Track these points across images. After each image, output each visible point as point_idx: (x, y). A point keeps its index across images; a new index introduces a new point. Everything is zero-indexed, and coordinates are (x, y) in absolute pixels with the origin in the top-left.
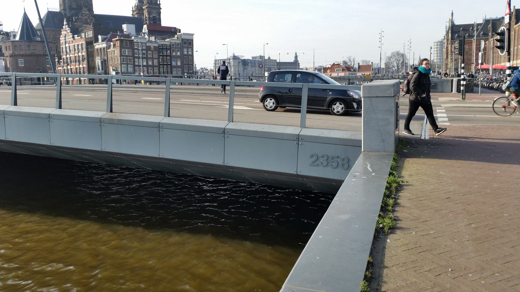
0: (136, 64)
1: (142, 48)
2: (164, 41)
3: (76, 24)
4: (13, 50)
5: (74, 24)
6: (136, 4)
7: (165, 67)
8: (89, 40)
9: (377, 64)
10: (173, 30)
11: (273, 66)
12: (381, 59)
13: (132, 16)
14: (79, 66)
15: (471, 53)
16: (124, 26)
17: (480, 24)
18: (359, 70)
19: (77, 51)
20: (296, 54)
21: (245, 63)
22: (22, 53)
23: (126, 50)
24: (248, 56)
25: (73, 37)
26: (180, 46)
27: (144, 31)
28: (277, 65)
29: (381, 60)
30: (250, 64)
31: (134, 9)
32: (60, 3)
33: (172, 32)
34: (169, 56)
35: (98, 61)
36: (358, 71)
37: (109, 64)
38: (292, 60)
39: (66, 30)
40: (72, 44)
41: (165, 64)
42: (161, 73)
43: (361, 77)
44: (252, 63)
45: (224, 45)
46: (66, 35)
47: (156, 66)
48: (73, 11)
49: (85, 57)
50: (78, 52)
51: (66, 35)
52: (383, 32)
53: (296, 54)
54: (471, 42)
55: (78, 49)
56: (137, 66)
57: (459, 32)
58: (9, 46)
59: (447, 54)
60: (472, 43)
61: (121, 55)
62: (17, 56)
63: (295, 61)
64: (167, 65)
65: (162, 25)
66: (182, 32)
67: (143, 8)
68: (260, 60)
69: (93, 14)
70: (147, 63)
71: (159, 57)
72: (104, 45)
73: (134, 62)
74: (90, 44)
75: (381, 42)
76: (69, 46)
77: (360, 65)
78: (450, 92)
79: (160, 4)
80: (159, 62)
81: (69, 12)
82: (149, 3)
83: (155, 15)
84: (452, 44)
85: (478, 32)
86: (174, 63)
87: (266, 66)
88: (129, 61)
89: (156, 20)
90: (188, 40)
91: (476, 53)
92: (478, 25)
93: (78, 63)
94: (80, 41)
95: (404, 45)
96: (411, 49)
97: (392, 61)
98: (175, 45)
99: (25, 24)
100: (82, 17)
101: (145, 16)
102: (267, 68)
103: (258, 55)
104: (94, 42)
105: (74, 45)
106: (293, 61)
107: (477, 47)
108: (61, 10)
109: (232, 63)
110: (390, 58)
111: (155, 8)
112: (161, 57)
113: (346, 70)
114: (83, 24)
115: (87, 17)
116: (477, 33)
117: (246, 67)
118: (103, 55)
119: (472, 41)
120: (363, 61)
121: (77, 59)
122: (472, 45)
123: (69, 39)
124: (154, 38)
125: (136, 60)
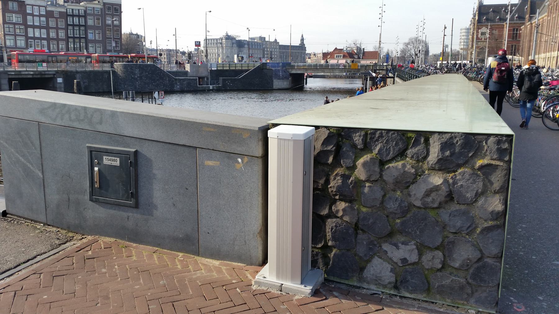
0: (29, 36)
1: (39, 13)
2: (78, 5)
7: (77, 40)
9: (391, 51)
11: (275, 49)
15: (500, 40)
17: (515, 5)
18: (363, 57)
20: (302, 36)
21: (240, 44)
23: (14, 15)
24: (244, 36)
26: (102, 12)
28: (280, 49)
30: (246, 46)
34: (83, 26)
36: (362, 59)
42: (70, 49)
43: (345, 66)
45: (140, 9)
47: (62, 40)
52: (385, 5)
53: (302, 36)
54: (503, 27)
57: (488, 13)
59: (473, 41)
60: (503, 28)
64: (80, 38)
68: (259, 41)
70: (48, 34)
75: (381, 19)
78: (250, 263)
84: (479, 29)
85: (512, 14)
86: (90, 36)
91: (508, 41)
92: (513, 5)
96: (424, 31)
97: (410, 49)
103: (258, 36)
106: (298, 45)
107: (510, 33)
110: (407, 44)
112: (70, 28)
113: (347, 57)
116: (511, 16)
117: (242, 49)
119: (504, 26)
122: (503, 31)
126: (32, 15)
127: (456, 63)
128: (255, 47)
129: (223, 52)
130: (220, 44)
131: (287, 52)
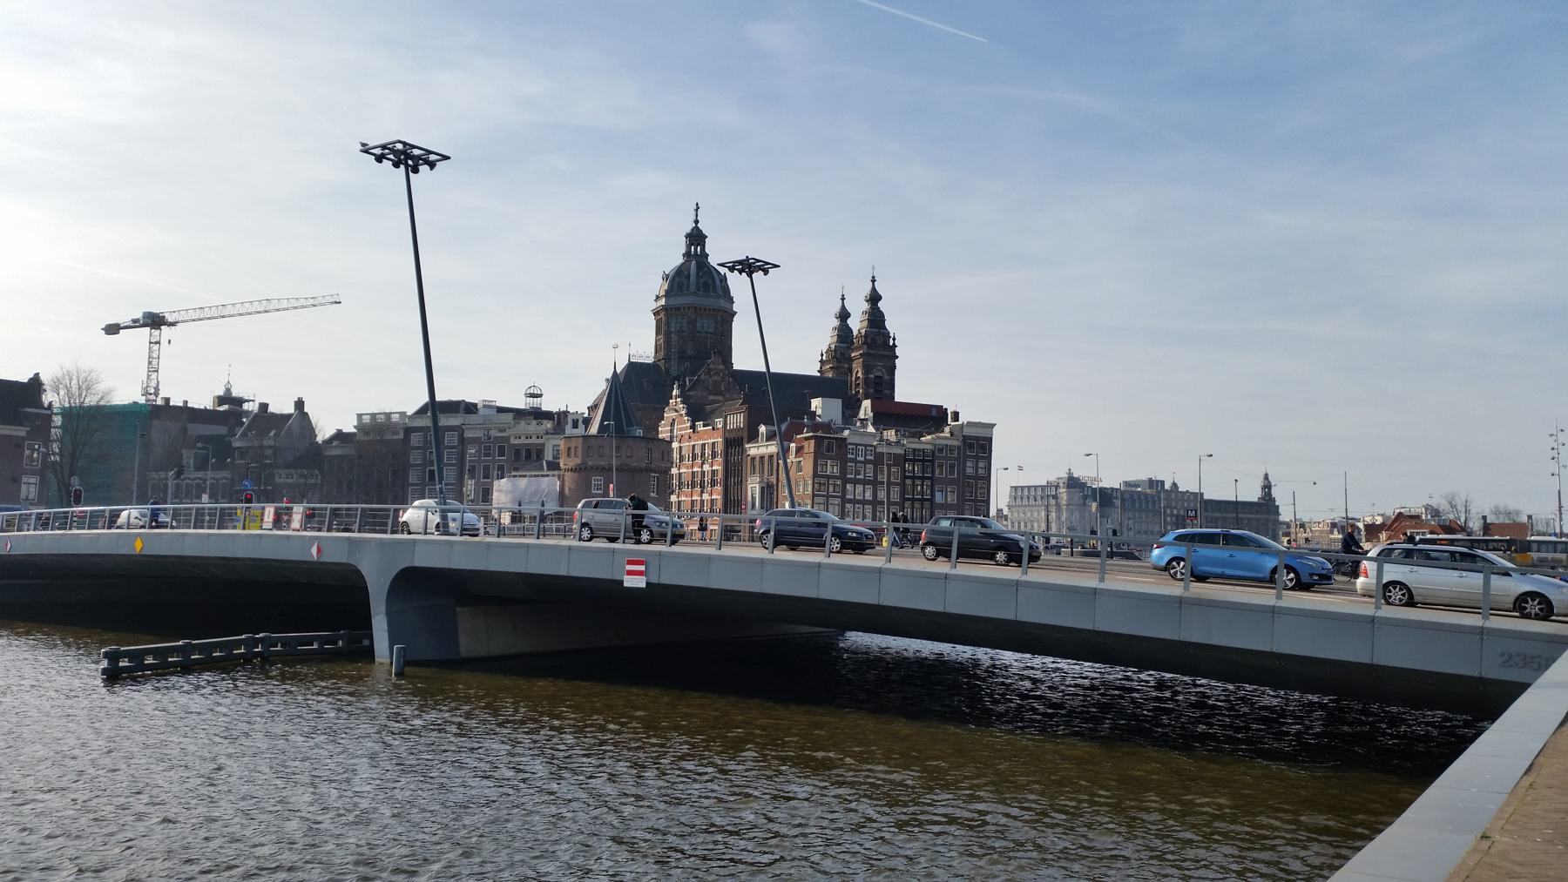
0: (847, 497)
1: (865, 458)
3: (691, 393)
4: (583, 457)
5: (688, 393)
6: (833, 346)
7: (917, 505)
8: (732, 436)
9: (1544, 521)
10: (934, 413)
12: (1560, 511)
13: (819, 374)
14: (701, 496)
16: (816, 403)
19: (699, 461)
21: (1105, 497)
22: (603, 463)
23: (829, 461)
25: (693, 427)
27: (861, 415)
29: (1561, 514)
31: (824, 358)
32: (656, 342)
33: (933, 417)
35: (753, 487)
37: (794, 493)
38: (1252, 494)
39: (675, 410)
40: (687, 444)
41: (918, 500)
44: (1125, 500)
46: (674, 420)
48: (686, 364)
49: (720, 476)
50: (703, 463)
51: (674, 420)
52: (1562, 430)
55: (703, 454)
56: (850, 501)
58: (576, 448)
61: (815, 475)
62: (601, 471)
63: (1263, 498)
64: (922, 500)
65: (897, 399)
66: (963, 419)
67: (852, 355)
68: (1148, 491)
69: (731, 371)
70: (875, 494)
71: (904, 482)
72: (772, 448)
73: (844, 491)
74: (734, 444)
76: (680, 447)
77: (1488, 521)
79: (895, 346)
80: (903, 492)
81: (676, 366)
82: (868, 344)
83: (880, 374)
86: (939, 498)
87: (1168, 511)
88: (831, 489)
89: (883, 385)
90: (977, 439)
93: (698, 489)
94: (711, 437)
95: (1554, 453)
98: (946, 451)
99: (613, 398)
100: (708, 377)
101: (856, 374)
102: (1172, 515)
104: (745, 440)
105: (694, 446)
106: (1256, 500)
108: (659, 360)
109: (1065, 498)
111: (883, 355)
112: (909, 482)
114: (709, 394)
115: (719, 379)
118: (766, 473)
120: (1497, 512)
121: (698, 479)
123: (681, 429)
124: (893, 433)
125: (849, 487)
126: (855, 461)
127: (879, 332)
128: (1141, 505)
129: (1059, 518)
130: (1053, 498)
131: (1225, 518)
